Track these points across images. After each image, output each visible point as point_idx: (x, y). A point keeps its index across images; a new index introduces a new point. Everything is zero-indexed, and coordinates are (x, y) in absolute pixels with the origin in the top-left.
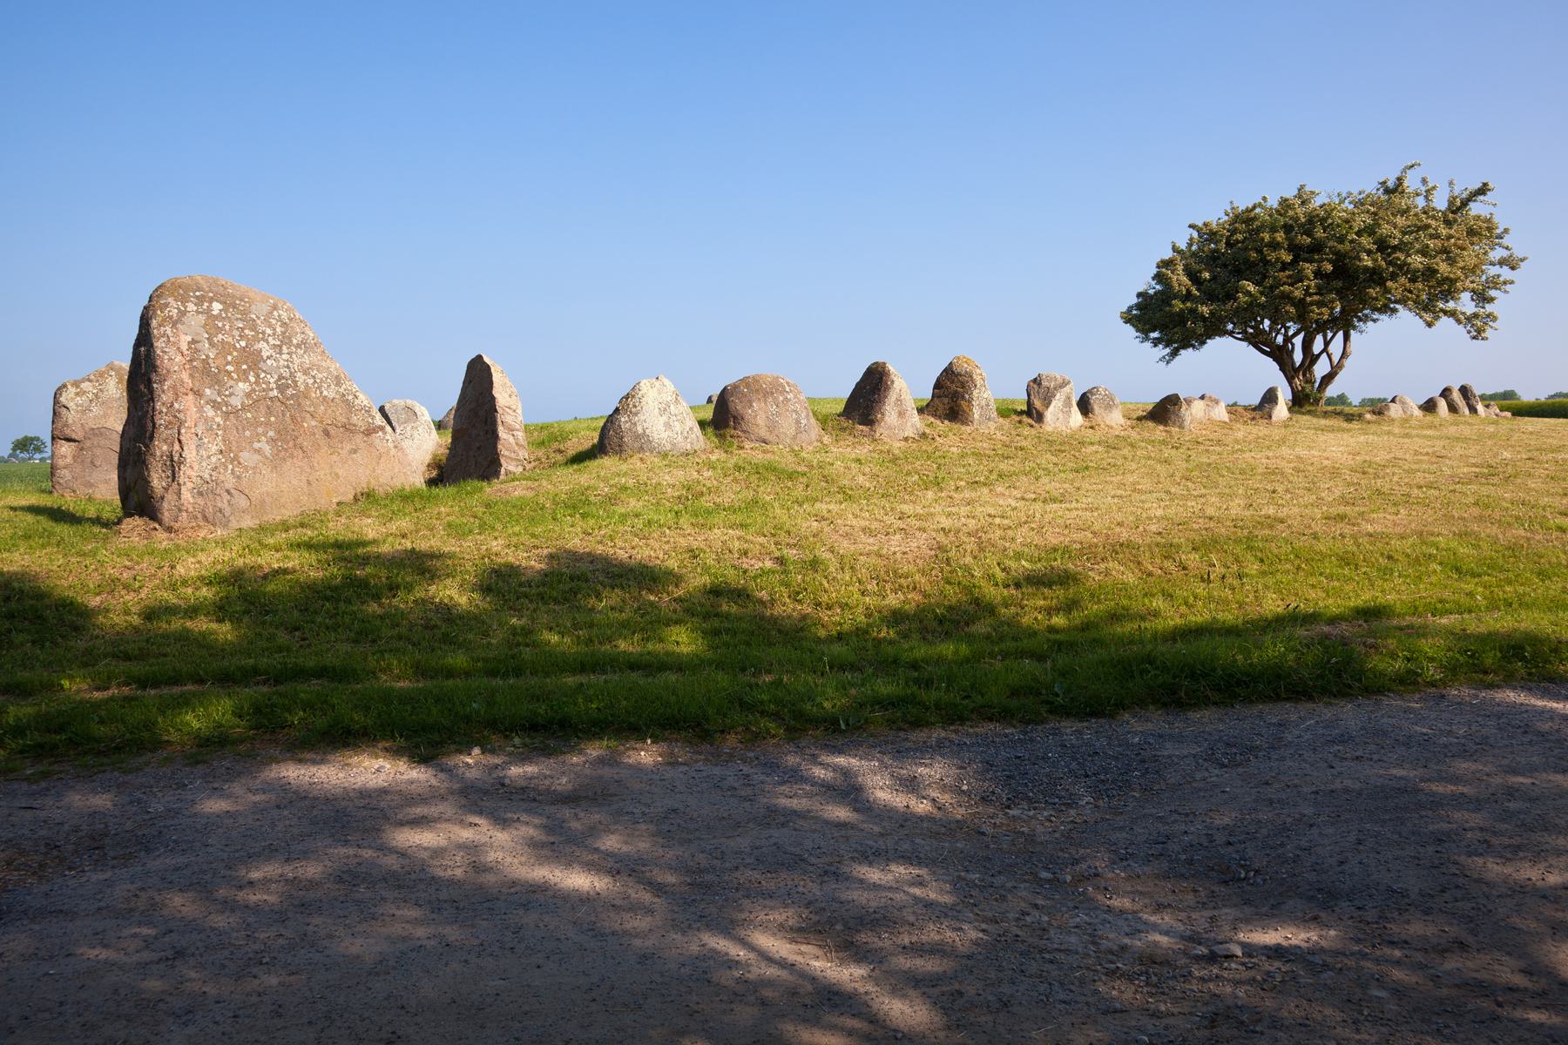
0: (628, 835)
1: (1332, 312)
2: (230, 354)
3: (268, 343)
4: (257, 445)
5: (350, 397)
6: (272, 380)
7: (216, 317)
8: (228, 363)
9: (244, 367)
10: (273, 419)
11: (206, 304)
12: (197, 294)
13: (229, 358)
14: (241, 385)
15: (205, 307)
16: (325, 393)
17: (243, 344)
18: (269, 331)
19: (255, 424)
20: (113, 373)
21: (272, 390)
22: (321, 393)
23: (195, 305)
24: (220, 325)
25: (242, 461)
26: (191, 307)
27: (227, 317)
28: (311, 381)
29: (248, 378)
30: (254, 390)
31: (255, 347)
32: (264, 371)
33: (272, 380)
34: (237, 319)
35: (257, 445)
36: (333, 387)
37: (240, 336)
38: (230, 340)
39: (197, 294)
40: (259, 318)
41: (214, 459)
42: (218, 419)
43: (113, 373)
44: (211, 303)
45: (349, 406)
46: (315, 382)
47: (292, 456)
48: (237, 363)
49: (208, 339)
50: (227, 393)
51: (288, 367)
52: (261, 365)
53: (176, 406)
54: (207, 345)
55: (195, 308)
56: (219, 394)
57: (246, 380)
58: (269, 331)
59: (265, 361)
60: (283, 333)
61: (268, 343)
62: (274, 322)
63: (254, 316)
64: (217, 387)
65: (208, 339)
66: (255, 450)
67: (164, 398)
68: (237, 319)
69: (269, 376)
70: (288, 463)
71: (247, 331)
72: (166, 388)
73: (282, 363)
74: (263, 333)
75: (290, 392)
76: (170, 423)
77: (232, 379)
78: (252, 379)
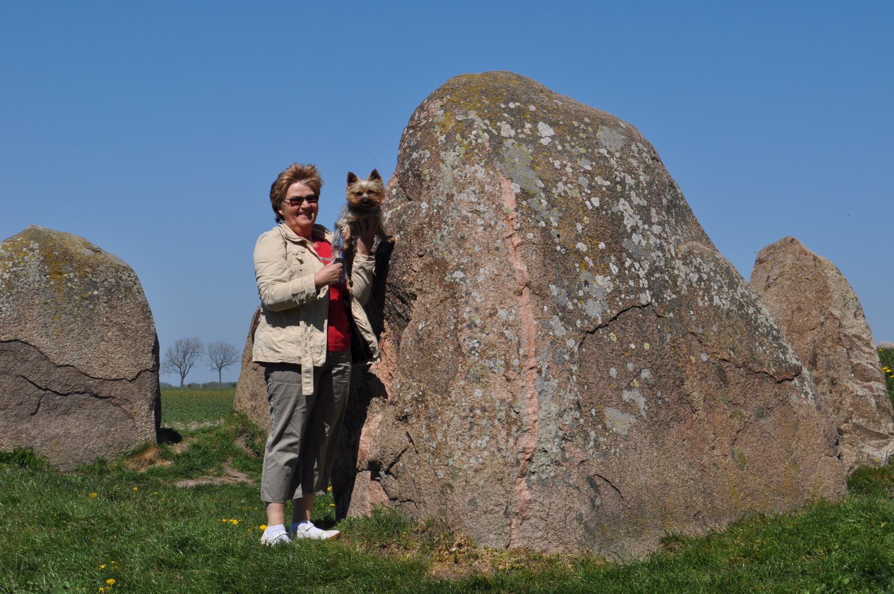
0: (88, 417)
1: (648, 241)
2: (581, 221)
3: (630, 202)
4: (626, 395)
5: (751, 310)
6: (642, 273)
7: (549, 150)
8: (578, 238)
9: (602, 245)
10: (647, 346)
11: (528, 126)
12: (512, 105)
13: (579, 227)
14: (599, 278)
15: (527, 131)
16: (716, 300)
17: (596, 201)
18: (629, 180)
19: (622, 354)
20: (36, 246)
21: (642, 290)
22: (711, 300)
23: (513, 126)
24: (557, 164)
25: (609, 425)
26: (506, 130)
27: (564, 150)
28: (695, 277)
29: (608, 267)
30: (617, 291)
31: (615, 209)
32: (630, 256)
33: (642, 273)
34: (580, 156)
35: (626, 395)
36: (726, 289)
37: (590, 187)
38: (575, 193)
39: (512, 105)
40: (612, 156)
41: (568, 419)
42: (571, 343)
43: (36, 246)
44: (535, 123)
45: (751, 323)
46: (700, 279)
47: (677, 419)
48: (591, 237)
49: (544, 190)
50: (581, 293)
51: (661, 248)
52: (625, 242)
53: (502, 313)
54: (545, 203)
55: (513, 133)
56: (570, 295)
57: (606, 271)
58: (629, 180)
59: (630, 237)
60: (650, 184)
61: (630, 202)
62: (635, 163)
63: (603, 151)
64: (566, 283)
65: (544, 190)
66: (626, 405)
67: (478, 297)
68: (580, 156)
69: (637, 265)
70: (673, 431)
71: (599, 180)
72: (480, 279)
73: (653, 241)
74: (622, 182)
75: (669, 295)
76: (492, 346)
77: (586, 266)
78: (615, 269)
